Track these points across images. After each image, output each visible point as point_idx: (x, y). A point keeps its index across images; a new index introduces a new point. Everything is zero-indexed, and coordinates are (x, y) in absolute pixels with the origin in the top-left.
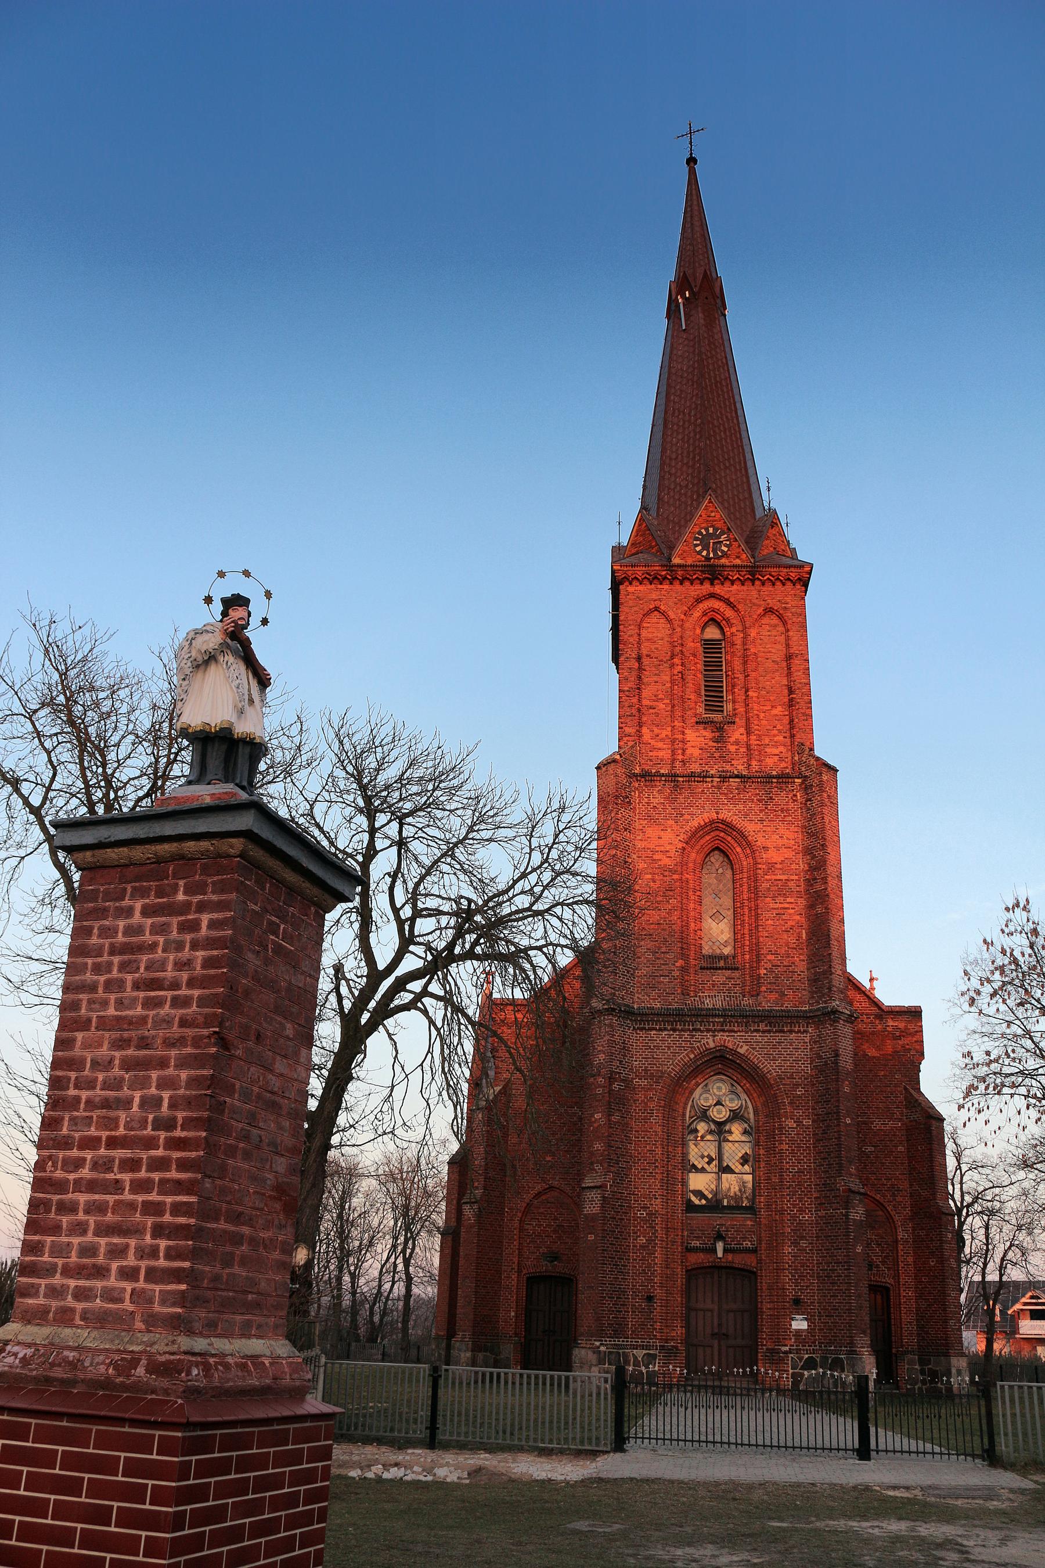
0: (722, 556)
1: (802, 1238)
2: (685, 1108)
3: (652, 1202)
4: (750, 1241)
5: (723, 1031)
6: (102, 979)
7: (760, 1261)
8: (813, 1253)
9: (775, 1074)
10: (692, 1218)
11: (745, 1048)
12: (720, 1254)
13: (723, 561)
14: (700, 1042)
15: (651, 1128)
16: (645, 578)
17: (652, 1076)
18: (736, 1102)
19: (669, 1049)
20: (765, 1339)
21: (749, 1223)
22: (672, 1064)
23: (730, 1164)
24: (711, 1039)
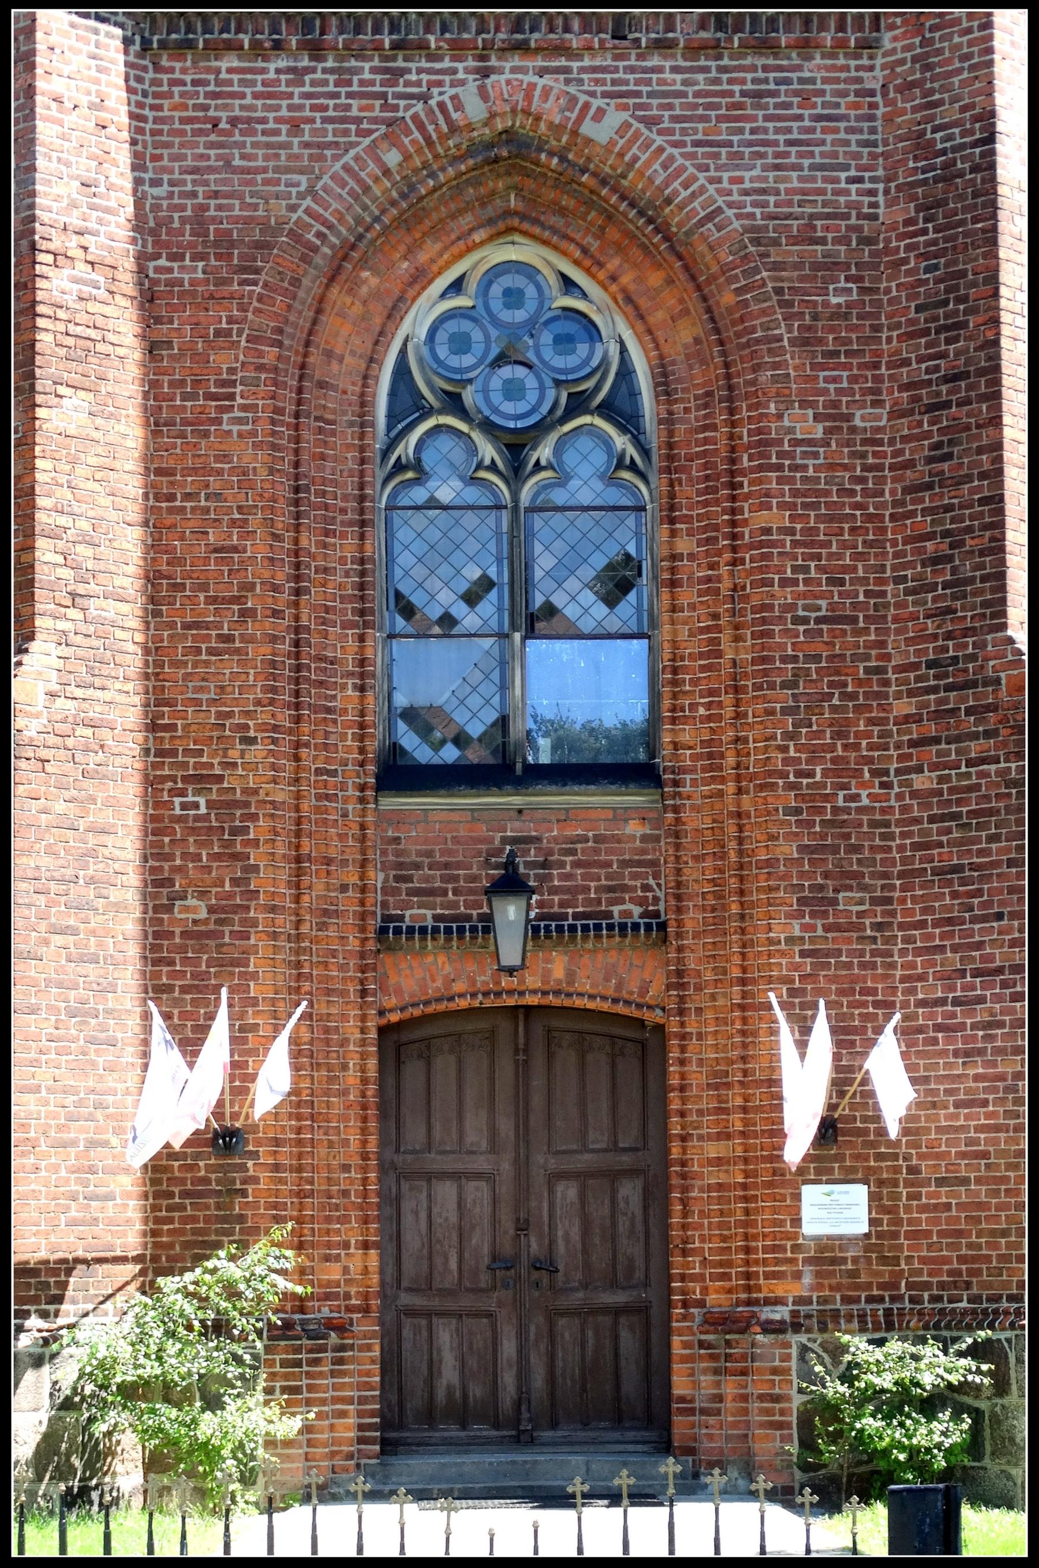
1: (847, 879)
2: (367, 378)
3: (234, 755)
4: (641, 902)
5: (522, 47)
6: (991, 1108)
7: (678, 979)
8: (891, 940)
9: (736, 224)
10: (398, 818)
11: (615, 118)
12: (510, 953)
14: (424, 98)
15: (225, 458)
17: (225, 243)
18: (583, 349)
19: (295, 126)
20: (701, 1277)
21: (634, 828)
22: (311, 191)
23: (559, 600)
24: (472, 86)
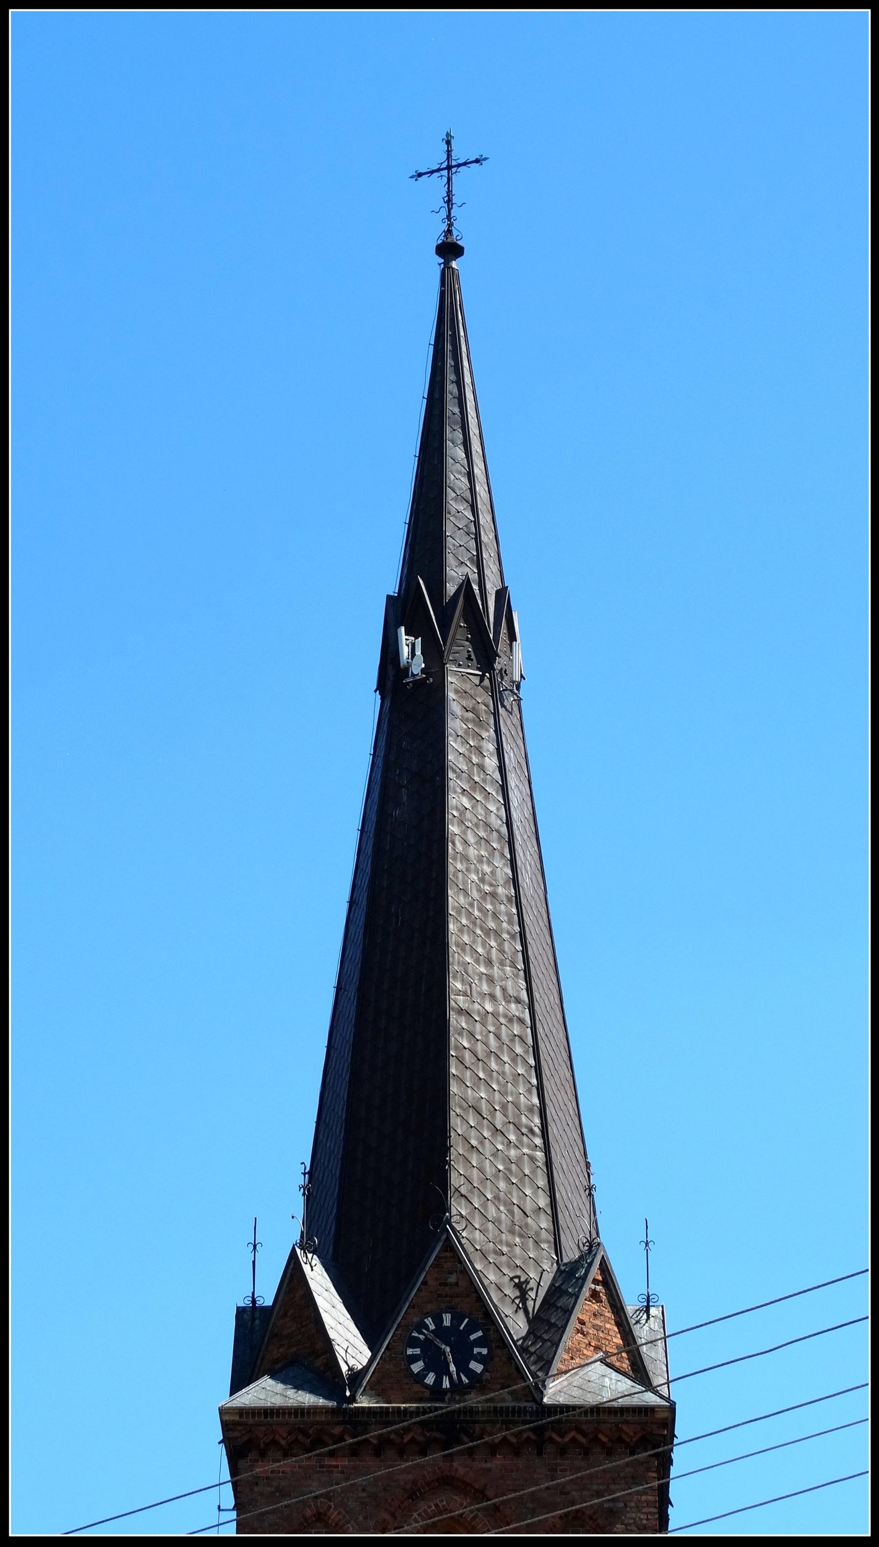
0: (470, 1387)
13: (474, 1400)
16: (296, 1441)
